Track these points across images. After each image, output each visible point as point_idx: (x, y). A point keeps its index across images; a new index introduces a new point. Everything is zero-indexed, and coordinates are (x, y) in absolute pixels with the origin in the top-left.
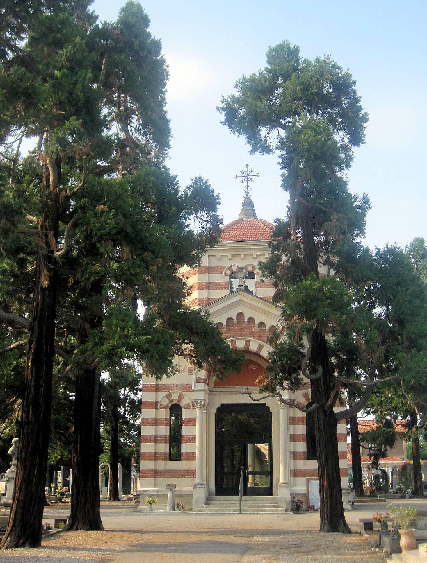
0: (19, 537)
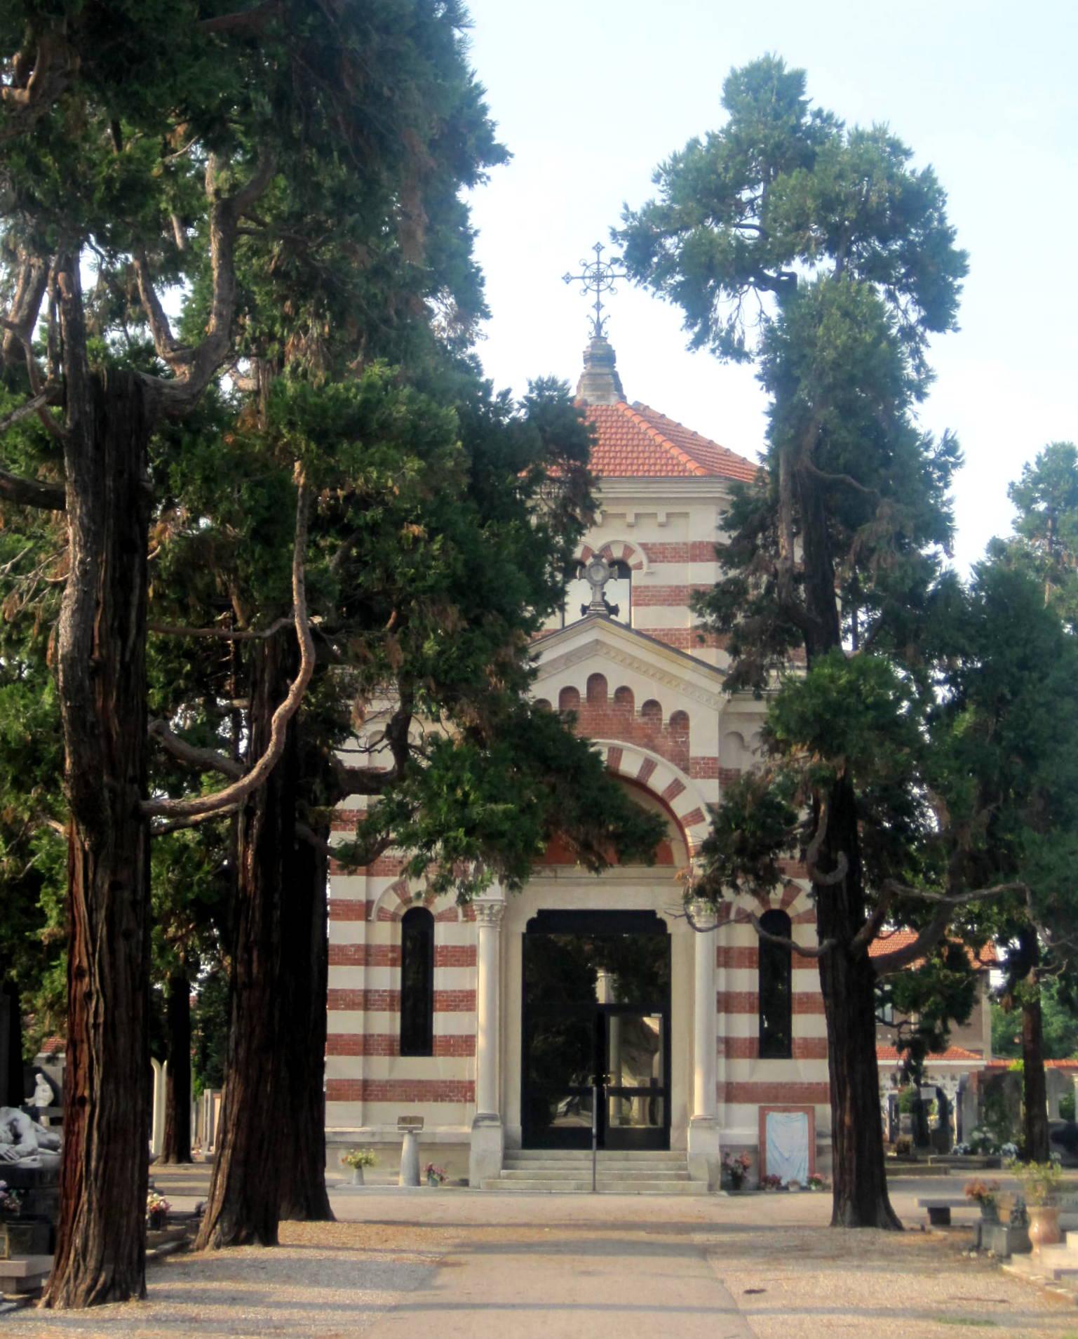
0: (238, 1225)
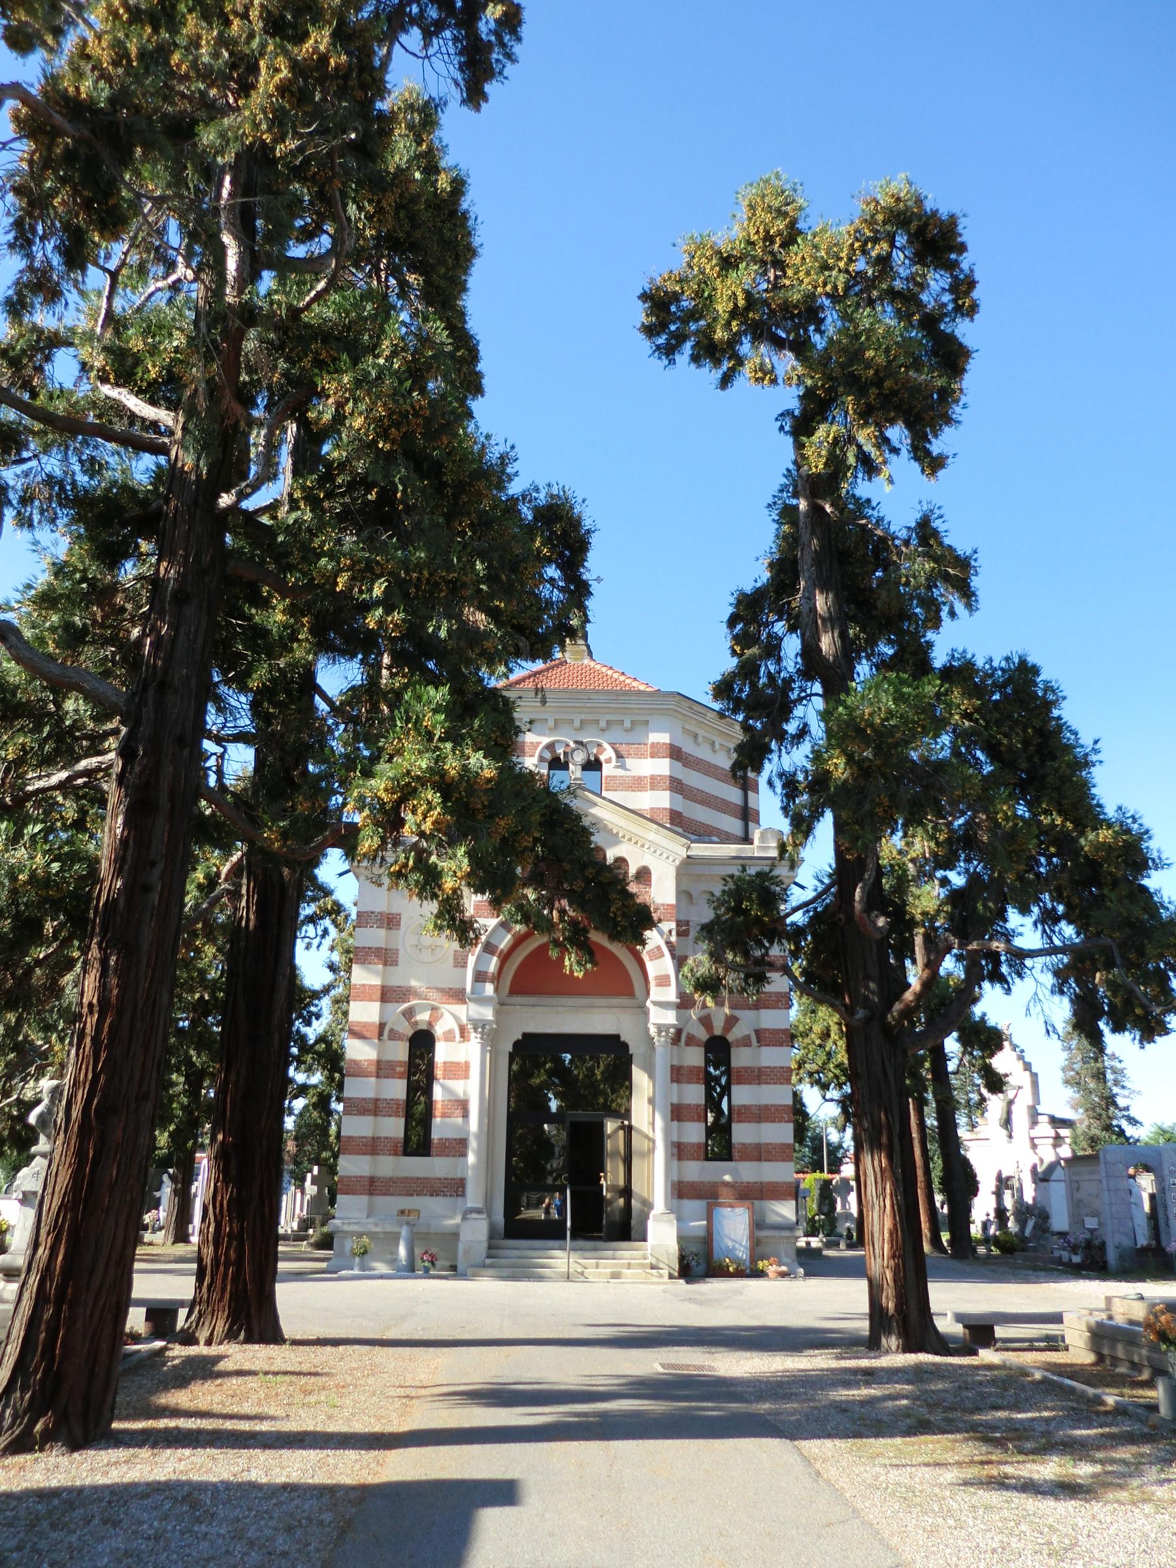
0: (34, 1411)
